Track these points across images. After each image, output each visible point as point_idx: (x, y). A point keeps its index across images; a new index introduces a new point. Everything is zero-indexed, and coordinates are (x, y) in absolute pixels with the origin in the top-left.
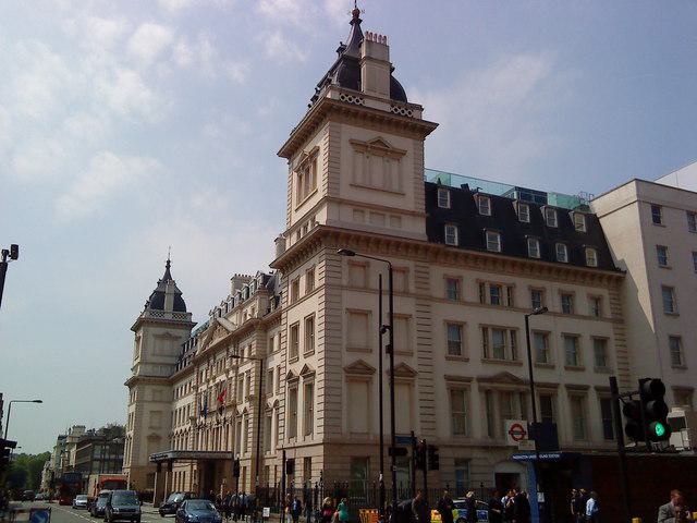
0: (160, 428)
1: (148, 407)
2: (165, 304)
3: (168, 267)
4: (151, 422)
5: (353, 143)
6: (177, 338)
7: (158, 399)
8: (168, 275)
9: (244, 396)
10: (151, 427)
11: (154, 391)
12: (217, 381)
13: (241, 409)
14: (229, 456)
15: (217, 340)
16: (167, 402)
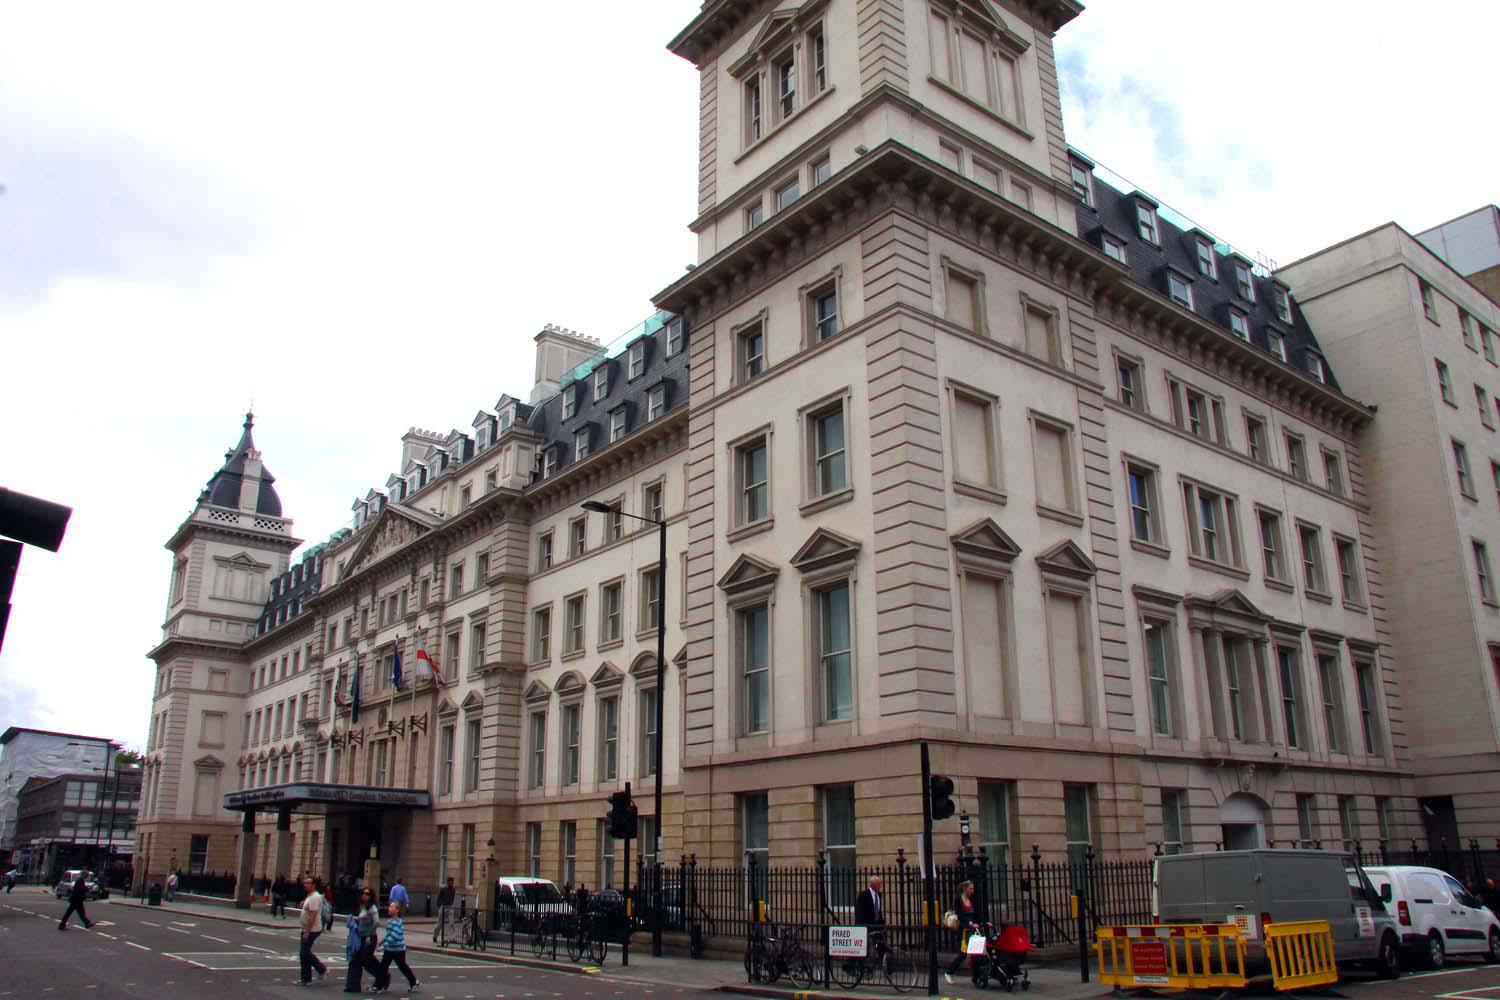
0: (220, 747)
1: (198, 703)
2: (238, 493)
3: (248, 426)
4: (203, 734)
5: (217, 559)
6: (267, 567)
7: (219, 687)
8: (247, 442)
9: (297, 718)
10: (202, 745)
11: (214, 671)
12: (383, 639)
13: (457, 696)
14: (423, 800)
15: (384, 553)
16: (238, 695)
